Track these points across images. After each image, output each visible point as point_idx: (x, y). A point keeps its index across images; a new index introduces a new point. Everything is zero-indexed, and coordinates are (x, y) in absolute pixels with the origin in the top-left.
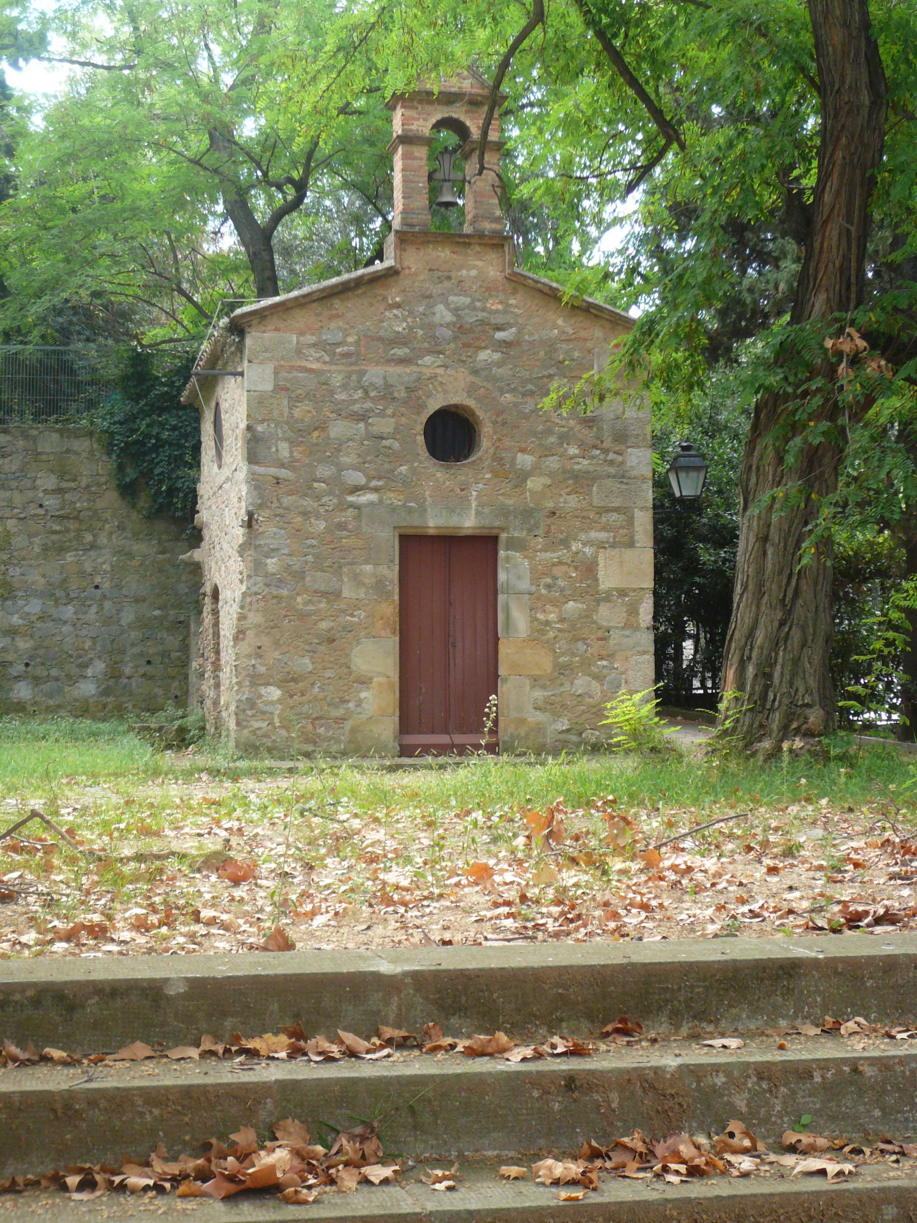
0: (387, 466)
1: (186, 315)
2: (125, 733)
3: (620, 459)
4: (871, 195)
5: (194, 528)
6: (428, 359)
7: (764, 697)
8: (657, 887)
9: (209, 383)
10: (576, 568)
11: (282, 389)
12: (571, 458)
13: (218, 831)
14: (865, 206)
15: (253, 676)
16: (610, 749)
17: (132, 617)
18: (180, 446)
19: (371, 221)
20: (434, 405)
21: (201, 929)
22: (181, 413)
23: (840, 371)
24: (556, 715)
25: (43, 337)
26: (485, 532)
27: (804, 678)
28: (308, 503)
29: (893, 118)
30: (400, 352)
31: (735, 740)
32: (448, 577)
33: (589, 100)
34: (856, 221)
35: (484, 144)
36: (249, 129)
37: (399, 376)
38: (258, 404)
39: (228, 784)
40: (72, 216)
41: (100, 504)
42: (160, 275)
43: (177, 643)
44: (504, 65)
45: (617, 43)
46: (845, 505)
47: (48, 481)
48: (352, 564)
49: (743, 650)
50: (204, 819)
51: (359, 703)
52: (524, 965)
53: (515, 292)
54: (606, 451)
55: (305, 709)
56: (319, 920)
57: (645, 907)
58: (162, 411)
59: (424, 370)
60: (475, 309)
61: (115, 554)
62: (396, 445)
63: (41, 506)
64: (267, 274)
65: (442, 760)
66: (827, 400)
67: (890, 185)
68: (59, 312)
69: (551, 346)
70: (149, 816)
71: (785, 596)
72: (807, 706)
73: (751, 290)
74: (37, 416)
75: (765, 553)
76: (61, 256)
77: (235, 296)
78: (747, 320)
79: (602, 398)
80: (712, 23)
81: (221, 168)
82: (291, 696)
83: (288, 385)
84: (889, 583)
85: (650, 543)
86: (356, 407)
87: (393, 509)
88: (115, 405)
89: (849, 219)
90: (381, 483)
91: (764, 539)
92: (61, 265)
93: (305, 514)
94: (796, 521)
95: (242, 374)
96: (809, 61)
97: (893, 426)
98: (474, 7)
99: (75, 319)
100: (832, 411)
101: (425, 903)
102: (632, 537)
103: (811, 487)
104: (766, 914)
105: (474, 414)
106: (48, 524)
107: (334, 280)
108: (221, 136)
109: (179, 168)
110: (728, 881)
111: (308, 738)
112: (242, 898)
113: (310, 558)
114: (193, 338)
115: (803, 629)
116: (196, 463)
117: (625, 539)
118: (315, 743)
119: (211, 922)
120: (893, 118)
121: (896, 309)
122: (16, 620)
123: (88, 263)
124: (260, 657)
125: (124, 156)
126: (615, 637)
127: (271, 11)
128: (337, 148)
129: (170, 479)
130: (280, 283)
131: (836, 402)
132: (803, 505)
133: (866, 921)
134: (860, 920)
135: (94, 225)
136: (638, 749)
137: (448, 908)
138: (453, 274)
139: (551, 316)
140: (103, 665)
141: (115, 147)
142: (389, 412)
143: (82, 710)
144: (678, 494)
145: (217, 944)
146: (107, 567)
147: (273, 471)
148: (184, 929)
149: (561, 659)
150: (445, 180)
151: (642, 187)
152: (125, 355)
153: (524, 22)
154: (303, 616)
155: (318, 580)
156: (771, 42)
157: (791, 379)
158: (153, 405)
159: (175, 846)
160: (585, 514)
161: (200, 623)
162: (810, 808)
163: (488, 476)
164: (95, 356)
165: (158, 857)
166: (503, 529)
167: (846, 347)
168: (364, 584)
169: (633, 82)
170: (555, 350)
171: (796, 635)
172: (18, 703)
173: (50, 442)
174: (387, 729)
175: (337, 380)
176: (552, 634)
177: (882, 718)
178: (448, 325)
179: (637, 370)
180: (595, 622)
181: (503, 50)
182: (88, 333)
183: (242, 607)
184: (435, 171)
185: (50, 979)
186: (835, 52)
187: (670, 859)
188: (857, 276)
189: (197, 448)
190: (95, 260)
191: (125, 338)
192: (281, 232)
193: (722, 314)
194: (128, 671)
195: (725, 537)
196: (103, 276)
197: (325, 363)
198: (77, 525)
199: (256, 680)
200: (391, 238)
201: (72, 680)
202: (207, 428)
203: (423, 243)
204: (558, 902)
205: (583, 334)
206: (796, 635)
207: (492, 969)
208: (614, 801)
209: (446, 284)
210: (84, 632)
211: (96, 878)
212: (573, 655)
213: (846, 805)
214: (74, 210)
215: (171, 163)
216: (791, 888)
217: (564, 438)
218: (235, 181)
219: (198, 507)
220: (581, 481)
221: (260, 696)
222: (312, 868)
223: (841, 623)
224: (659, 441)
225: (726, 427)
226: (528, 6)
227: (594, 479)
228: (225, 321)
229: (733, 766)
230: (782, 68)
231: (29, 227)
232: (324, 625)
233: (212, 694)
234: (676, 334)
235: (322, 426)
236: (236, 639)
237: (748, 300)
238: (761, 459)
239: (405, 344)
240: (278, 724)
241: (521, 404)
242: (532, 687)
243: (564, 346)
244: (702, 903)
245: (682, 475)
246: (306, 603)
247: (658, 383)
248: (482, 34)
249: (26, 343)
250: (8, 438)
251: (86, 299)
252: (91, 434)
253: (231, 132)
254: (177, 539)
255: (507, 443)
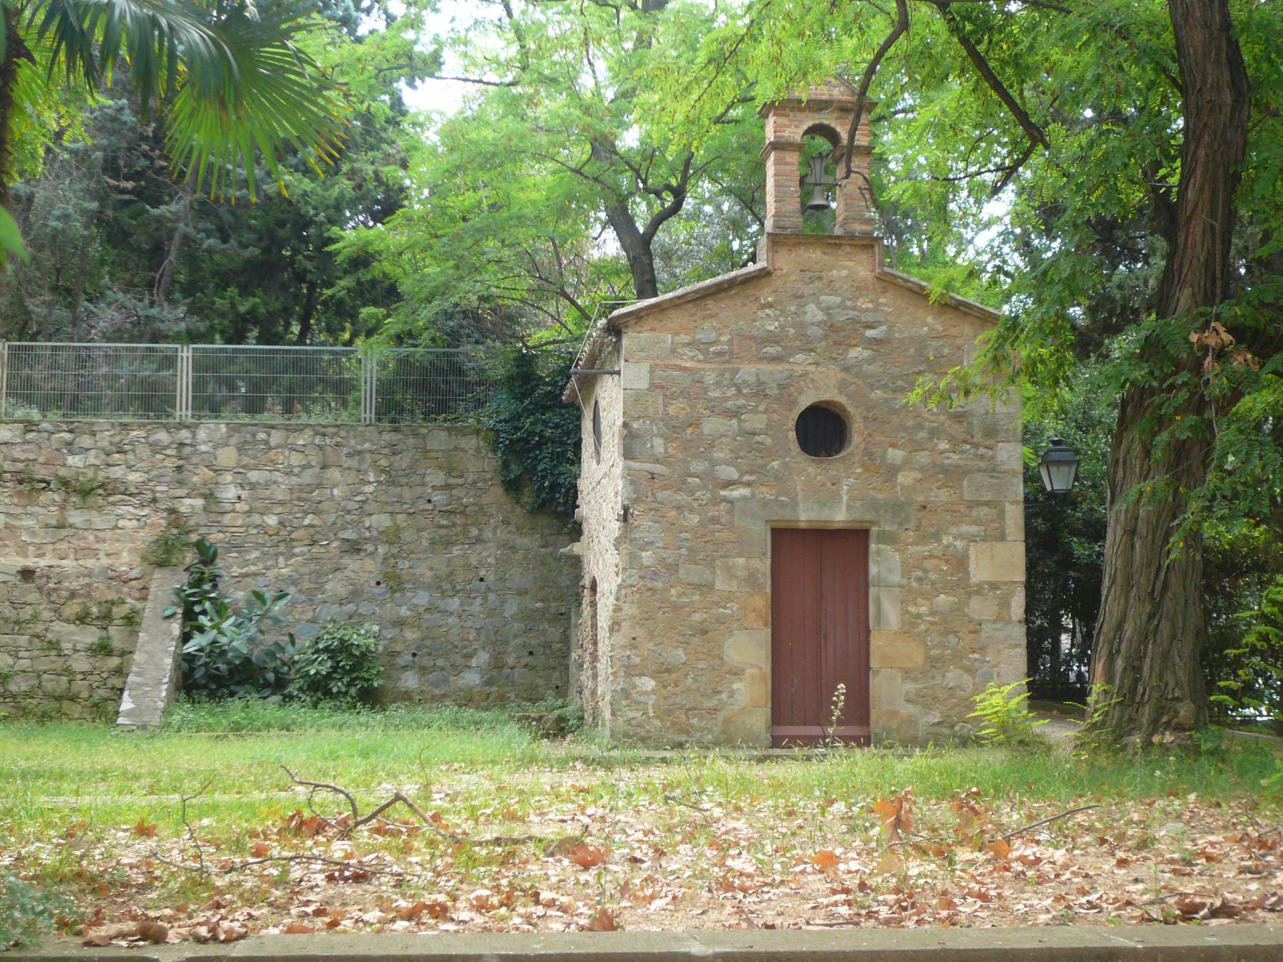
0: (759, 461)
1: (569, 316)
2: (506, 722)
3: (990, 453)
4: (1235, 192)
5: (575, 522)
6: (800, 357)
7: (1133, 690)
8: (1001, 877)
9: (589, 383)
10: (947, 561)
11: (657, 387)
12: (942, 453)
13: (581, 818)
14: (1228, 201)
15: (627, 667)
16: (978, 742)
17: (515, 609)
18: (562, 444)
19: (749, 226)
20: (805, 402)
21: (540, 910)
22: (563, 411)
23: (1206, 365)
24: (928, 708)
25: (433, 340)
26: (856, 526)
27: (1174, 672)
28: (681, 497)
29: (1255, 116)
30: (772, 350)
31: (1105, 734)
32: (818, 573)
33: (954, 104)
34: (1220, 215)
35: (852, 150)
36: (629, 140)
37: (771, 373)
38: (634, 401)
39: (601, 773)
40: (462, 224)
41: (486, 500)
42: (546, 280)
43: (558, 634)
44: (871, 71)
45: (981, 48)
46: (1214, 497)
47: (437, 478)
48: (726, 557)
49: (1111, 642)
50: (570, 806)
51: (732, 694)
52: (836, 949)
53: (885, 291)
54: (976, 446)
55: (678, 699)
56: (658, 904)
57: (983, 897)
58: (545, 409)
59: (796, 368)
60: (845, 308)
61: (499, 548)
62: (769, 441)
63: (429, 501)
64: (647, 277)
65: (806, 751)
66: (1193, 394)
67: (1253, 181)
68: (448, 316)
69: (921, 344)
70: (518, 802)
71: (1153, 590)
72: (1177, 699)
73: (1120, 287)
74: (427, 415)
75: (1133, 546)
76: (451, 263)
77: (616, 298)
78: (1117, 316)
79: (967, 393)
80: (1073, 27)
81: (607, 177)
82: (665, 687)
83: (663, 383)
84: (1266, 577)
85: (1021, 536)
86: (729, 404)
87: (765, 503)
88: (502, 404)
89: (1213, 215)
90: (753, 478)
91: (1132, 532)
92: (451, 271)
93: (679, 508)
94: (1164, 514)
95: (618, 373)
96: (1170, 62)
97: (1267, 419)
98: (841, 18)
99: (465, 323)
100: (1198, 405)
101: (765, 889)
102: (1003, 530)
103: (1179, 479)
104: (1104, 905)
105: (845, 410)
106: (437, 519)
107: (708, 282)
108: (603, 147)
109: (562, 178)
110: (1073, 873)
111: (676, 730)
112: (587, 882)
113: (684, 551)
114: (577, 339)
115: (1173, 623)
116: (577, 460)
117: (996, 533)
118: (688, 733)
119: (550, 904)
120: (1255, 116)
121: (1264, 305)
122: (404, 611)
123: (477, 269)
124: (635, 648)
125: (509, 167)
126: (987, 630)
127: (649, 27)
128: (712, 156)
129: (552, 475)
130: (659, 286)
131: (1203, 396)
132: (1171, 499)
133: (1202, 913)
134: (1197, 913)
135: (481, 233)
136: (1006, 743)
137: (787, 895)
138: (823, 274)
139: (921, 314)
140: (487, 656)
141: (499, 159)
142: (762, 408)
143: (466, 700)
144: (1049, 488)
145: (551, 925)
146: (491, 560)
147: (648, 466)
148: (521, 910)
149: (932, 652)
150: (816, 184)
151: (1011, 187)
152: (512, 356)
153: (889, 31)
154: (676, 608)
155: (689, 573)
156: (1131, 44)
157: (1157, 373)
158: (536, 404)
159: (536, 831)
160: (955, 508)
161: (579, 615)
162: (1177, 802)
163: (859, 470)
164: (486, 359)
165: (516, 842)
166: (873, 523)
167: (1212, 341)
168: (736, 577)
169: (997, 86)
170: (926, 347)
171: (1165, 627)
172: (406, 692)
173: (439, 439)
174: (759, 720)
175: (710, 378)
176: (923, 627)
177: (1263, 714)
178: (818, 325)
179: (1003, 365)
180: (967, 615)
181: (871, 57)
182: (477, 335)
183: (617, 599)
184: (806, 175)
185: (368, 953)
186: (1196, 54)
187: (1020, 849)
188: (1222, 271)
189: (578, 445)
190: (483, 267)
191: (513, 340)
192: (661, 236)
193: (1091, 311)
194: (511, 661)
195: (1096, 531)
196: (492, 281)
197: (699, 361)
198: (463, 520)
199: (630, 670)
200: (763, 240)
201: (457, 670)
202: (587, 425)
203: (795, 245)
204: (897, 891)
205: (953, 331)
206: (1165, 627)
207: (803, 953)
208: (978, 794)
209: (817, 284)
210: (469, 624)
211: (450, 860)
212: (945, 647)
213: (1214, 800)
214: (464, 219)
215: (554, 173)
216: (1136, 881)
217: (935, 433)
218: (615, 189)
219: (578, 502)
220: (951, 475)
221: (635, 687)
222: (663, 853)
223: (1218, 618)
224: (1029, 435)
225: (1100, 422)
226: (893, 15)
227: (966, 473)
228: (603, 321)
229: (1102, 760)
230: (1144, 69)
231: (421, 235)
232: (698, 617)
233: (590, 684)
234: (1041, 329)
235: (695, 423)
236: (611, 630)
237: (1118, 297)
238: (1128, 452)
239: (777, 342)
240: (651, 714)
241: (892, 399)
242: (904, 680)
243: (934, 343)
244: (1043, 893)
245: (1053, 469)
246: (680, 596)
247: (1023, 379)
248: (849, 43)
249: (416, 346)
250: (399, 436)
251: (475, 304)
252: (477, 432)
253: (613, 145)
254: (559, 533)
255: (878, 437)
